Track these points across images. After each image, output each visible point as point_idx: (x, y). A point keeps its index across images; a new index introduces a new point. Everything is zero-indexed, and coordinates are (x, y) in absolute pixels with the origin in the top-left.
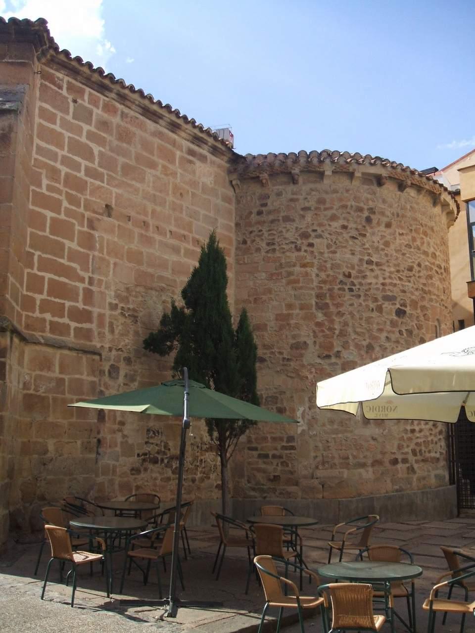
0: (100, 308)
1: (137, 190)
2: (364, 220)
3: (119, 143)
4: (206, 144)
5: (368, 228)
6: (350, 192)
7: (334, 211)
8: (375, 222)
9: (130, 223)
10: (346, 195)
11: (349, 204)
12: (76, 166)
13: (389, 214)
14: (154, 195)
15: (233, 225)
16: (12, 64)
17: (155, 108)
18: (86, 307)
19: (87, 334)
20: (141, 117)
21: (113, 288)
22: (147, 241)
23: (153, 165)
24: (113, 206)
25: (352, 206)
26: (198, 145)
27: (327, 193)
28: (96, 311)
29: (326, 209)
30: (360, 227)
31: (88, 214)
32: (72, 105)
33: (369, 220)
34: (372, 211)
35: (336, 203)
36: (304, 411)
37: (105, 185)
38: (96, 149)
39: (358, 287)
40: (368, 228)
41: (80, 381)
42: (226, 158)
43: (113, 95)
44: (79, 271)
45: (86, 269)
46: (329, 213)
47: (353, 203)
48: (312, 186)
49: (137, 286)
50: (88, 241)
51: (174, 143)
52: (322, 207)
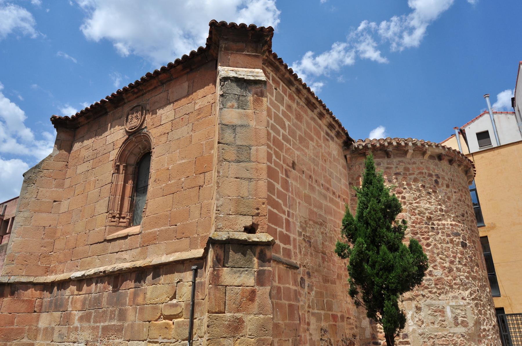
0: (294, 234)
1: (306, 154)
2: (434, 182)
3: (297, 121)
4: (335, 129)
5: (437, 187)
6: (423, 164)
7: (415, 176)
8: (440, 183)
9: (304, 175)
10: (421, 166)
11: (424, 171)
12: (278, 133)
13: (448, 180)
14: (314, 159)
15: (348, 184)
16: (249, 55)
17: (314, 101)
18: (287, 233)
19: (287, 253)
20: (306, 106)
21: (299, 220)
22: (312, 188)
23: (312, 139)
24: (296, 163)
25: (426, 173)
26: (330, 130)
27: (409, 164)
28: (292, 236)
29: (410, 174)
30: (432, 186)
31: (285, 166)
32: (274, 90)
33: (436, 182)
34: (437, 176)
35: (416, 170)
36: (413, 315)
37: (291, 147)
38: (287, 123)
39: (436, 226)
40: (437, 187)
41: (289, 288)
42: (342, 140)
43: (293, 89)
44: (282, 205)
45: (285, 205)
46: (412, 177)
47: (426, 171)
48: (400, 159)
49: (310, 220)
50: (286, 185)
51: (320, 126)
52: (408, 173)
